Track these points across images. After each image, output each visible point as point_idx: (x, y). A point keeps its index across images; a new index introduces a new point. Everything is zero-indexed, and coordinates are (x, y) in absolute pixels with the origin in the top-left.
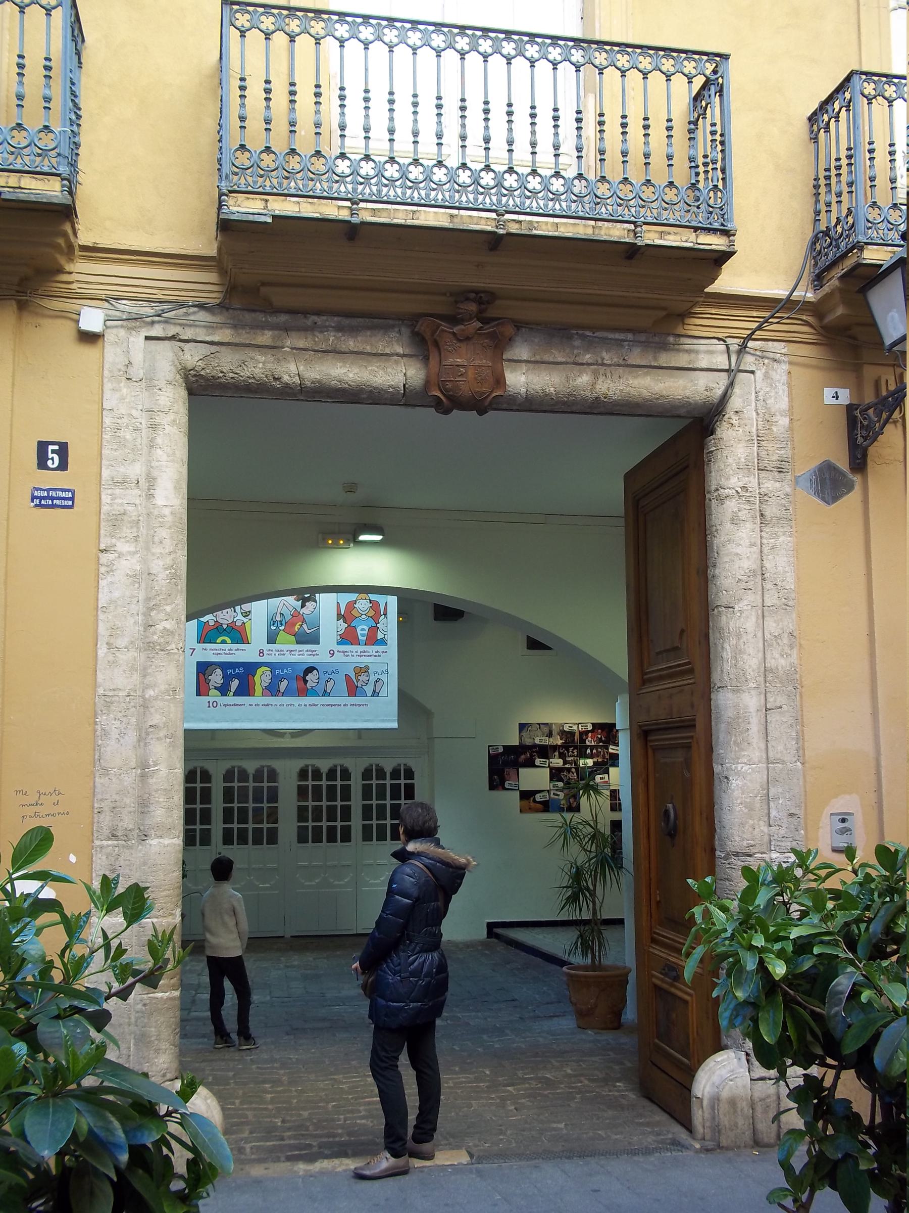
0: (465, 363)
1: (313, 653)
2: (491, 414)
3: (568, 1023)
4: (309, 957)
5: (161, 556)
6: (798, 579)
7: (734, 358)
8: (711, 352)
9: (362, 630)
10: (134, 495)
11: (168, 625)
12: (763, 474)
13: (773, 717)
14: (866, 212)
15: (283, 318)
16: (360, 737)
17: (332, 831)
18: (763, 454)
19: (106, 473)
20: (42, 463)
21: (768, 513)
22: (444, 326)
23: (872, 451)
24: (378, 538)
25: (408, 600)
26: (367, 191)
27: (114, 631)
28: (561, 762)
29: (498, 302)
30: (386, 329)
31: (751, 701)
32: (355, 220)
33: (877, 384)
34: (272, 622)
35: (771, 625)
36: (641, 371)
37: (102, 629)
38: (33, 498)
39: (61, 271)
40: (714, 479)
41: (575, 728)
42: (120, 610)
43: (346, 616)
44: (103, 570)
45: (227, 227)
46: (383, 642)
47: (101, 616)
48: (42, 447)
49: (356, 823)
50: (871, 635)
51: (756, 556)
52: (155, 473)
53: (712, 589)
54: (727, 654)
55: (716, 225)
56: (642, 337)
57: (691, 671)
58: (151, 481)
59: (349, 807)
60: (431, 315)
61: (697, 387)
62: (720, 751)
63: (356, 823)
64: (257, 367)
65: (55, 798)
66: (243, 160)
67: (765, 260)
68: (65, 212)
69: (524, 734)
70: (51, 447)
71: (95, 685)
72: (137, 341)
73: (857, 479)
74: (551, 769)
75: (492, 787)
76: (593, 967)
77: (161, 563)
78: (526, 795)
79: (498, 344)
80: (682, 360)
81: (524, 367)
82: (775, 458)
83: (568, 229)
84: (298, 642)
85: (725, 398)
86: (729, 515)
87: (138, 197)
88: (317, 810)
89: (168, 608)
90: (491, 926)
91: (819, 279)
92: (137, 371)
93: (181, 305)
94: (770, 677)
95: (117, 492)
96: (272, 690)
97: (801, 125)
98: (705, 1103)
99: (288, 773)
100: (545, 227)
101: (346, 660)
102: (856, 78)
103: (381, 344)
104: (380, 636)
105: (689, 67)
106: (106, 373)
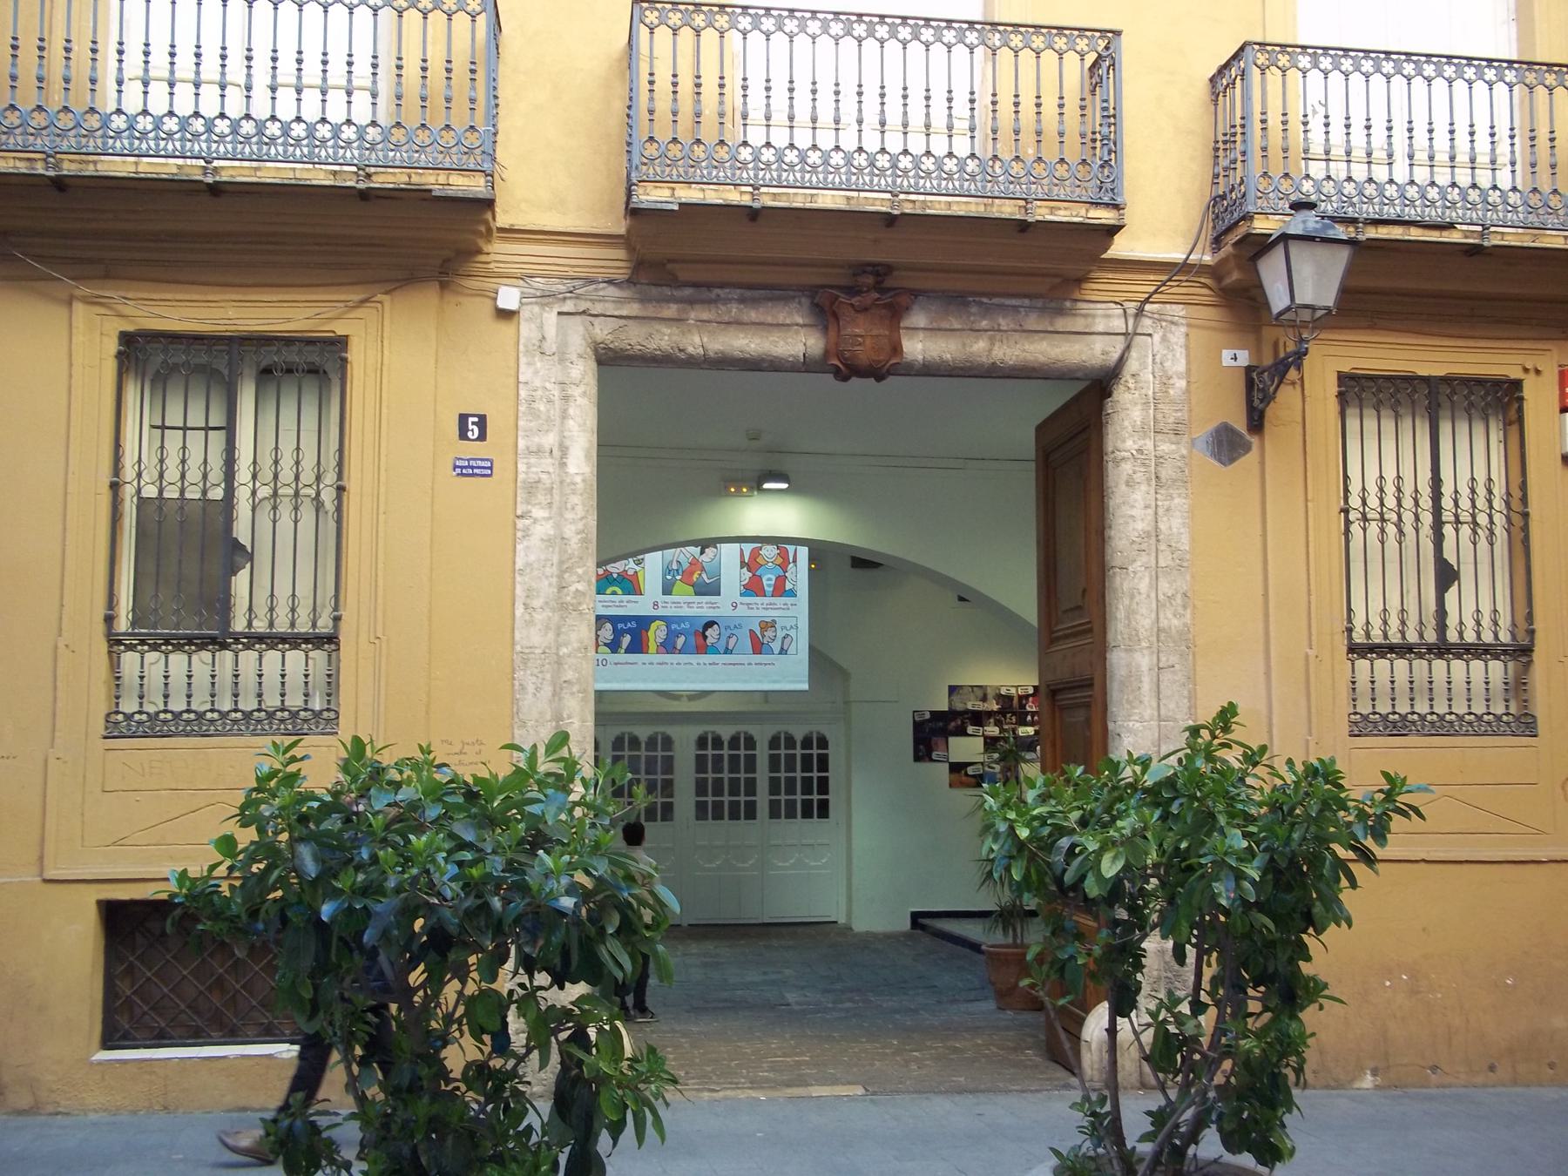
0: (862, 334)
1: (713, 606)
2: (891, 379)
3: (990, 1005)
4: (709, 946)
5: (573, 522)
6: (1193, 540)
7: (1131, 322)
8: (1108, 316)
9: (768, 581)
10: (547, 463)
11: (580, 587)
12: (1159, 437)
13: (1166, 677)
14: (1256, 182)
15: (688, 292)
16: (767, 701)
17: (734, 806)
18: (1159, 416)
19: (522, 443)
20: (463, 435)
21: (1163, 474)
22: (843, 298)
23: (1269, 413)
24: (785, 486)
25: (820, 552)
26: (768, 176)
27: (530, 593)
28: (997, 730)
29: (896, 273)
30: (786, 300)
31: (1144, 661)
32: (756, 205)
33: (1276, 345)
34: (667, 570)
35: (1164, 585)
36: (1036, 337)
37: (519, 590)
38: (455, 467)
39: (480, 252)
40: (1110, 443)
41: (1013, 691)
42: (536, 573)
43: (751, 564)
44: (519, 534)
45: (634, 213)
46: (792, 593)
47: (518, 579)
48: (463, 419)
49: (762, 799)
50: (1266, 595)
51: (1150, 518)
52: (567, 443)
53: (1109, 551)
54: (1121, 614)
55: (1106, 200)
56: (1039, 303)
57: (1090, 630)
58: (564, 451)
59: (754, 779)
60: (831, 287)
61: (1094, 352)
62: (1113, 709)
63: (762, 799)
64: (663, 339)
65: (477, 747)
66: (651, 150)
67: (1160, 220)
68: (488, 204)
69: (954, 698)
70: (471, 420)
71: (513, 644)
72: (551, 317)
73: (1254, 440)
74: (986, 738)
75: (917, 758)
76: (1015, 945)
77: (573, 528)
78: (957, 768)
79: (895, 313)
80: (1079, 324)
81: (921, 335)
82: (1171, 420)
83: (962, 207)
84: (697, 594)
85: (1121, 361)
86: (1124, 477)
87: (549, 179)
88: (718, 783)
89: (580, 571)
90: (916, 917)
91: (1217, 242)
92: (551, 345)
93: (590, 281)
94: (1162, 636)
95: (533, 460)
96: (668, 647)
97: (1201, 89)
98: (1094, 1046)
99: (685, 739)
100: (939, 206)
101: (750, 613)
102: (1248, 49)
103: (782, 314)
104: (788, 586)
105: (1082, 44)
106: (521, 348)
